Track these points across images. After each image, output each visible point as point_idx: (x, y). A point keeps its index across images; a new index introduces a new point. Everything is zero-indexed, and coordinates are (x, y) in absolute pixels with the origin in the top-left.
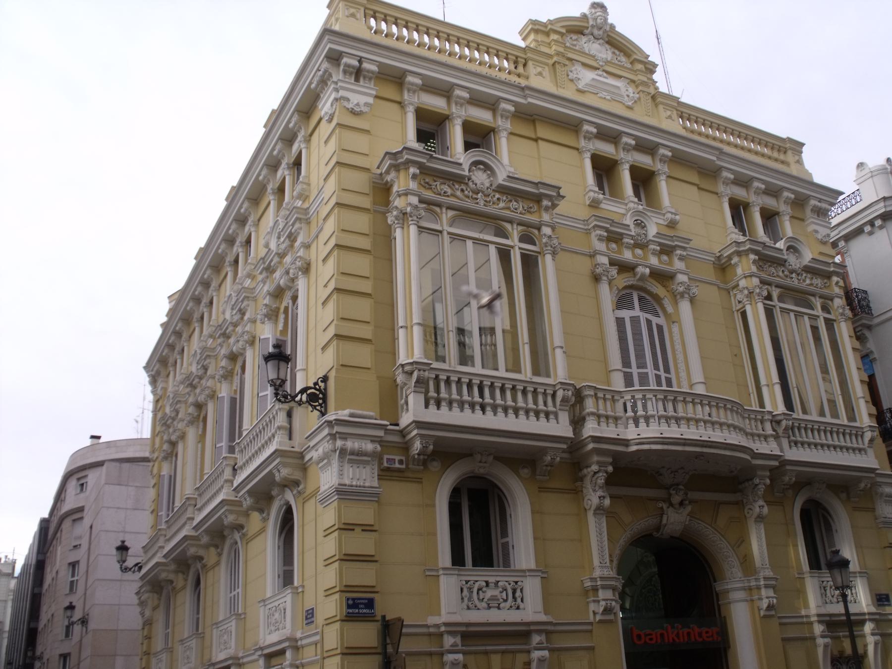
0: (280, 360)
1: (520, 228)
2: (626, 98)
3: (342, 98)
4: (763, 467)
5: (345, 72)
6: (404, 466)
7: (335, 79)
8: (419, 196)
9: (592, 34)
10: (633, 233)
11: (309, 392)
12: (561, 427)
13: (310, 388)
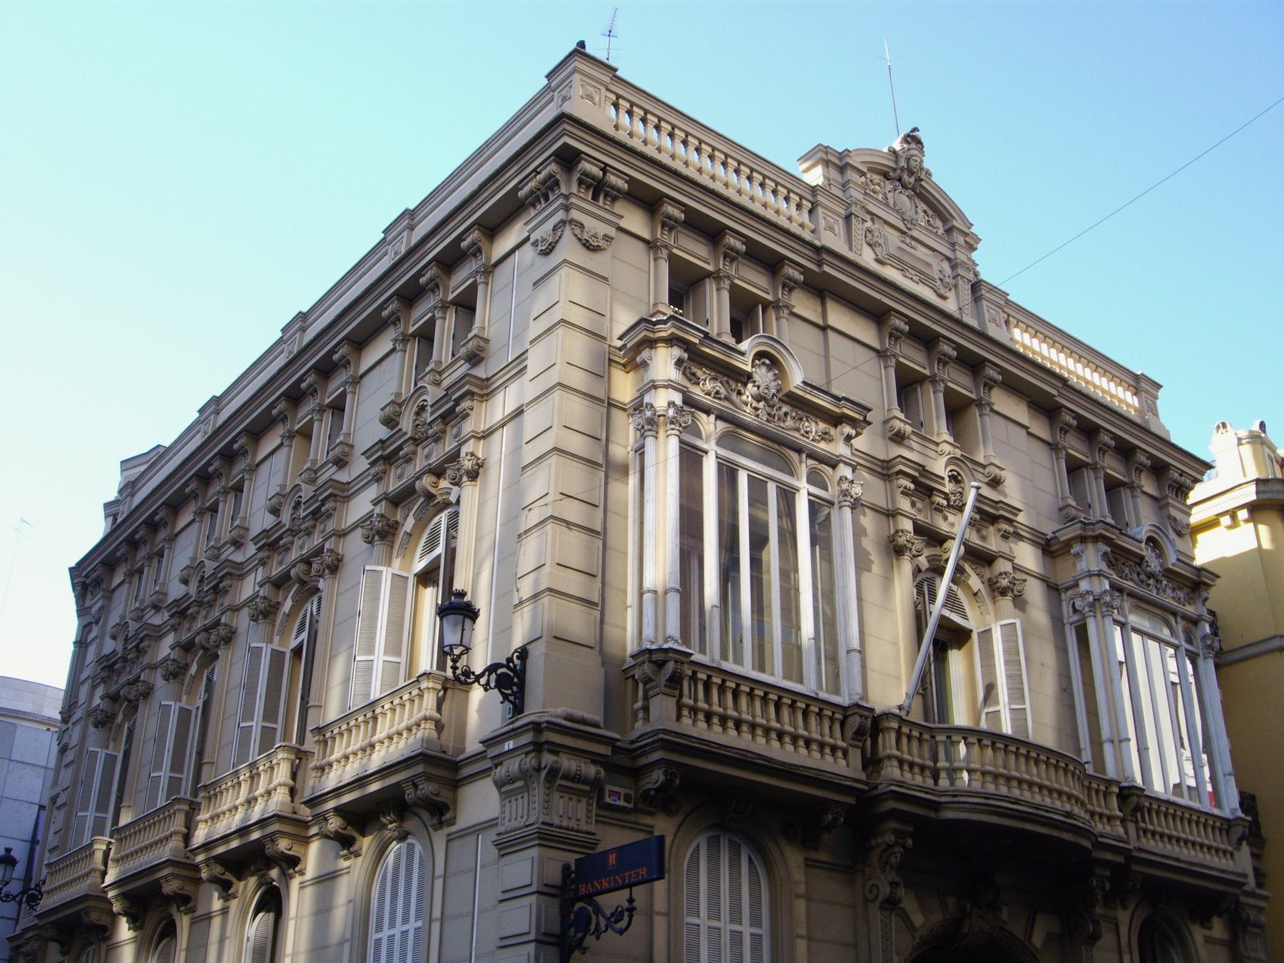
0: (466, 616)
1: (810, 462)
2: (939, 283)
3: (572, 221)
4: (1106, 864)
5: (580, 182)
6: (631, 806)
7: (563, 190)
8: (684, 393)
9: (900, 180)
10: (946, 490)
11: (500, 671)
12: (846, 767)
13: (501, 665)
